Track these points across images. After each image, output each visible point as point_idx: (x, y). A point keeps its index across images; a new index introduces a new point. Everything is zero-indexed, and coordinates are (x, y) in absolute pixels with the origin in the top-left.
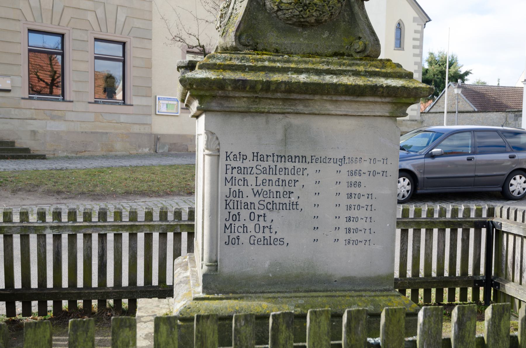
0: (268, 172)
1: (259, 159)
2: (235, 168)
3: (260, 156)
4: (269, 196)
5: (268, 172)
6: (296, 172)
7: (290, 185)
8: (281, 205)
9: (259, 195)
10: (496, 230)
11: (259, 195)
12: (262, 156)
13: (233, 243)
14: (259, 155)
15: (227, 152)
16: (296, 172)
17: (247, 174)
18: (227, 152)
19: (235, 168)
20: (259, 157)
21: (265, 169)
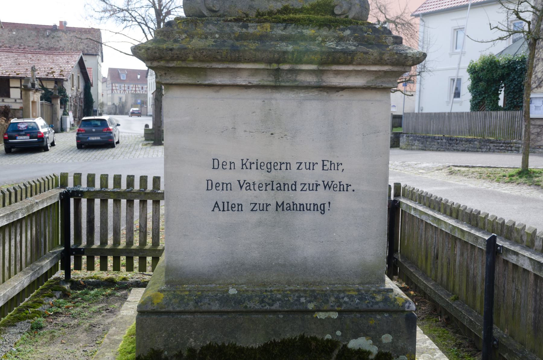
0: (282, 188)
1: (285, 209)
2: (284, 163)
3: (287, 205)
4: (279, 168)
5: (282, 188)
6: (272, 166)
7: (276, 168)
8: (225, 185)
9: (330, 188)
10: (402, 210)
11: (330, 188)
12: (278, 185)
13: (269, 164)
14: (285, 204)
15: (242, 160)
16: (272, 166)
17: (305, 163)
18: (242, 160)
19: (284, 163)
20: (285, 206)
21: (288, 205)
